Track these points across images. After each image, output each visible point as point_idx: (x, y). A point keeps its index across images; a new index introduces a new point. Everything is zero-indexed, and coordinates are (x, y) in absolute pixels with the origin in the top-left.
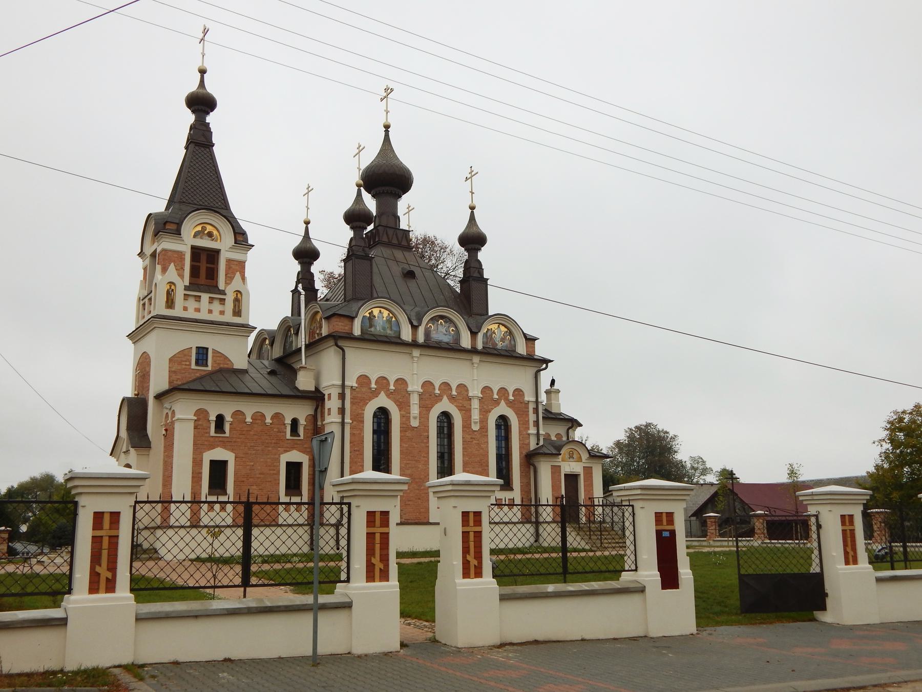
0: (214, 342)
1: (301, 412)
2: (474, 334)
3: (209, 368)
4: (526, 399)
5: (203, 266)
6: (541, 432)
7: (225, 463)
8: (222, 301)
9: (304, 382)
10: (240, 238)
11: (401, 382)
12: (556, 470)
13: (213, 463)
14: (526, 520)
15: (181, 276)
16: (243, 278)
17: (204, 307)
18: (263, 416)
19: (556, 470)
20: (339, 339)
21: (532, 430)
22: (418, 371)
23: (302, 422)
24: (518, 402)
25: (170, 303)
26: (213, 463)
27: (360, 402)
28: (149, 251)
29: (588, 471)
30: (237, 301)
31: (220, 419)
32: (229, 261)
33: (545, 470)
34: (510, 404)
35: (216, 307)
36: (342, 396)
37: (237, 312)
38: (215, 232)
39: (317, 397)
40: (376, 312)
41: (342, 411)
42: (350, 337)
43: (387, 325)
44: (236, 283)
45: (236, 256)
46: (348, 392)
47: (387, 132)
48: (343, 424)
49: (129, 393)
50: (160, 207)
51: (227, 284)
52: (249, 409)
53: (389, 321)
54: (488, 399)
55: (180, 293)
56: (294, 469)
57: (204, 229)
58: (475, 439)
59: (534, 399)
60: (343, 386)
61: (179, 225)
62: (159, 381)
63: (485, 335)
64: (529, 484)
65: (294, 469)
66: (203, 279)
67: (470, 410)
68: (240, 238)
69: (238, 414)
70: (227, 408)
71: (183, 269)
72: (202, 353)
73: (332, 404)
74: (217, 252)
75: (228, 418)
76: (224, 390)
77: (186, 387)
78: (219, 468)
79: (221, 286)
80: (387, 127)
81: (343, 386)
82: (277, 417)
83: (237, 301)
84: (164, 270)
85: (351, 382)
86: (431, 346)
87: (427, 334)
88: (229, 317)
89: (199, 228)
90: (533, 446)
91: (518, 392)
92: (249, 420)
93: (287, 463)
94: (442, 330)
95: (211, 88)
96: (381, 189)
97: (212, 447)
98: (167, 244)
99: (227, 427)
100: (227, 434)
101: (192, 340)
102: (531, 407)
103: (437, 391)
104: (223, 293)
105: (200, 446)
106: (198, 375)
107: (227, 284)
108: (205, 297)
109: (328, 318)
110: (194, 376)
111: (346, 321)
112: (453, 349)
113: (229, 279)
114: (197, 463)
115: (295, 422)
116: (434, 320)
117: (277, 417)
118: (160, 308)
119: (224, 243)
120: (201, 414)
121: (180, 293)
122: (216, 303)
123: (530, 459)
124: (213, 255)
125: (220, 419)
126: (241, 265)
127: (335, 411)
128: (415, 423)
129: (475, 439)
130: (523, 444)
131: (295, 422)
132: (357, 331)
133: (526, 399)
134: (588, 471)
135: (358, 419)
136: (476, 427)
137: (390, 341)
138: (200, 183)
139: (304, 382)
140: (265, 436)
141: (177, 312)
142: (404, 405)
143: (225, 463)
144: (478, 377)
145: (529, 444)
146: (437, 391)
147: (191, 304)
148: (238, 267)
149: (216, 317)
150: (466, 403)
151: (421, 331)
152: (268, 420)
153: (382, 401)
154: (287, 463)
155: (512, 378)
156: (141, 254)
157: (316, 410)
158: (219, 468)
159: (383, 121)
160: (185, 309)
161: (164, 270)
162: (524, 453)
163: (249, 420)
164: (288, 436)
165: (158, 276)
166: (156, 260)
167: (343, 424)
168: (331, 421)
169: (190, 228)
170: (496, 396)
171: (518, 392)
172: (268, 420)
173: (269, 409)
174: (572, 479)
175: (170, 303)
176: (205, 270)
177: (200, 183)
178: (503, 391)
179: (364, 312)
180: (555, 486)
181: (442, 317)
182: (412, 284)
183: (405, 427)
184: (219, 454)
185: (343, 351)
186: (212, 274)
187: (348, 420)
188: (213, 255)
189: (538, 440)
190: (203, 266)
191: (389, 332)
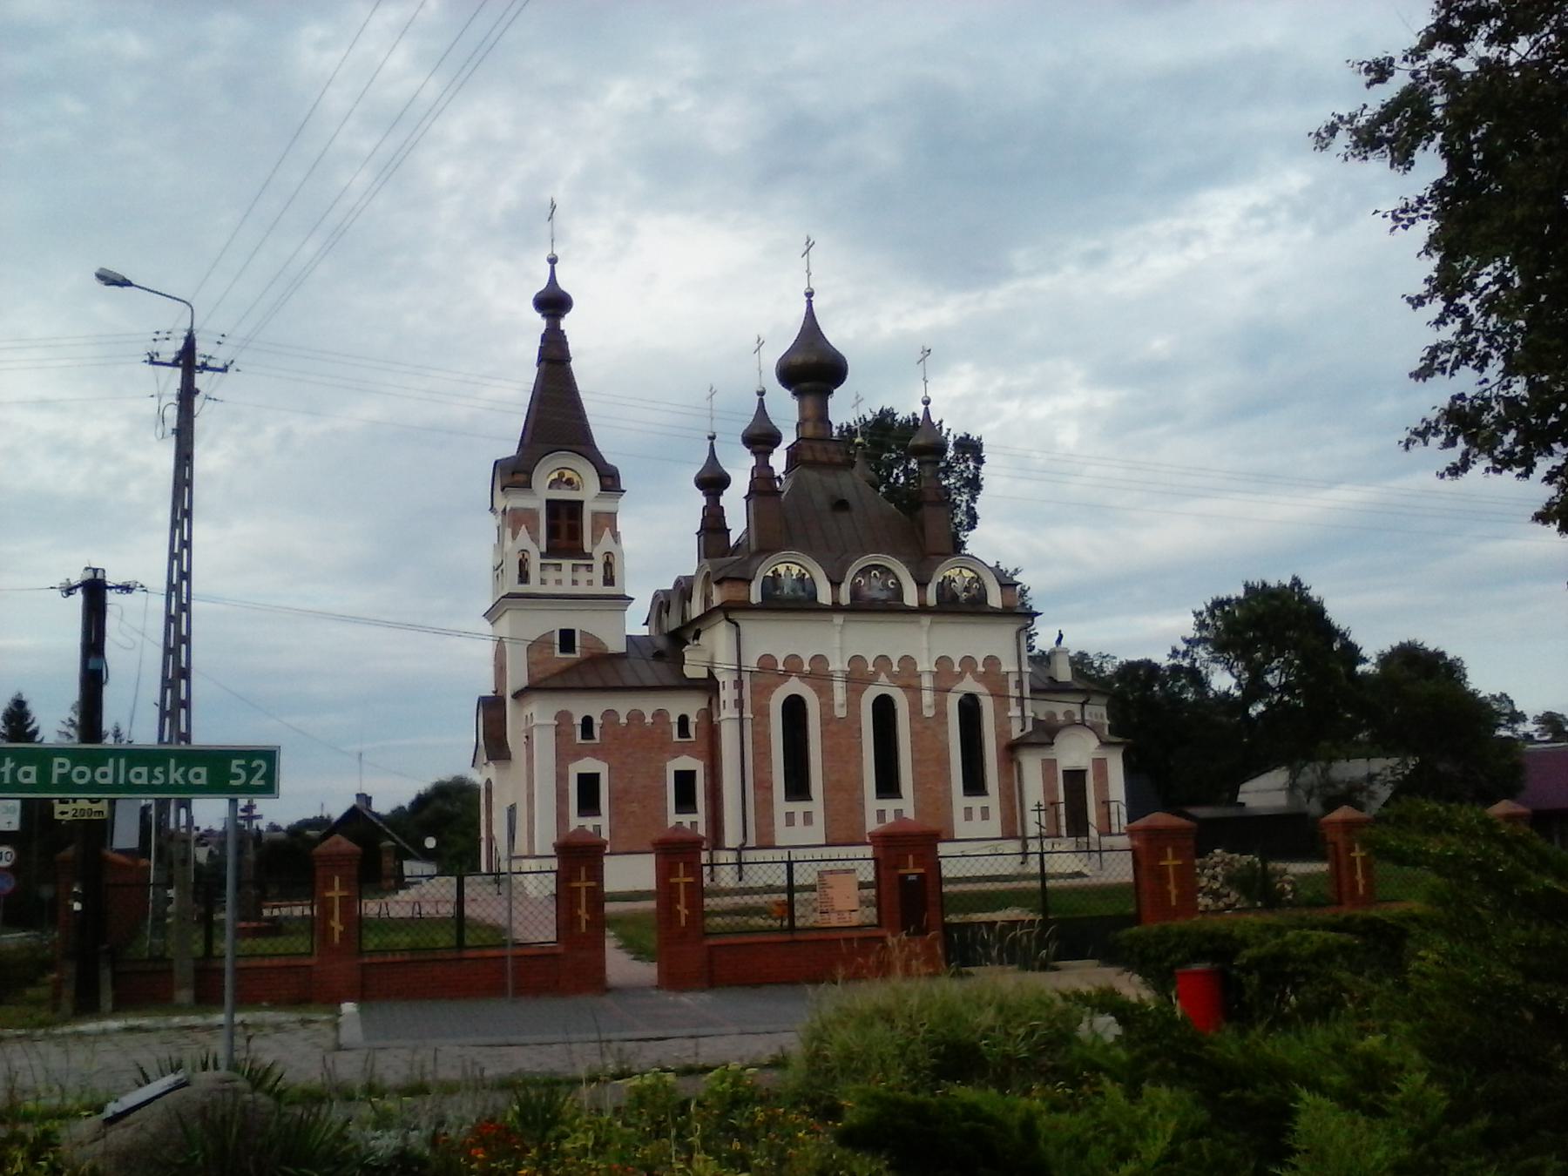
0: (582, 621)
1: (691, 706)
2: (922, 585)
3: (578, 655)
4: (1004, 669)
5: (564, 524)
6: (1029, 713)
7: (692, 774)
8: (589, 567)
9: (694, 669)
10: (610, 481)
11: (819, 659)
12: (1049, 766)
13: (581, 777)
14: (1009, 835)
15: (535, 540)
16: (616, 536)
17: (564, 577)
18: (641, 715)
19: (1049, 766)
20: (731, 610)
21: (1015, 712)
22: (839, 643)
23: (693, 719)
24: (992, 672)
25: (524, 577)
26: (581, 777)
27: (762, 693)
28: (499, 506)
29: (1100, 765)
30: (608, 565)
31: (587, 723)
32: (595, 515)
33: (1031, 765)
34: (980, 678)
35: (583, 575)
36: (739, 684)
37: (609, 580)
38: (576, 479)
39: (709, 686)
40: (782, 569)
41: (739, 703)
42: (746, 607)
43: (799, 586)
44: (606, 542)
45: (605, 506)
46: (746, 678)
47: (810, 303)
48: (741, 719)
49: (488, 691)
50: (510, 449)
51: (594, 543)
52: (623, 706)
53: (801, 578)
54: (945, 672)
55: (535, 562)
56: (685, 781)
57: (561, 475)
58: (927, 730)
59: (1016, 669)
60: (739, 670)
61: (529, 473)
62: (517, 677)
63: (941, 586)
64: (1011, 786)
65: (685, 781)
66: (563, 541)
67: (920, 689)
68: (609, 482)
69: (609, 714)
70: (593, 707)
71: (537, 529)
72: (567, 638)
73: (727, 694)
74: (581, 502)
75: (597, 721)
76: (611, 684)
77: (543, 685)
78: (588, 784)
79: (587, 548)
80: (810, 295)
81: (739, 670)
82: (660, 715)
83: (608, 565)
84: (514, 535)
85: (751, 662)
86: (861, 607)
87: (855, 592)
88: (599, 588)
89: (555, 476)
90: (1016, 733)
91: (992, 661)
92: (623, 720)
93: (677, 772)
94: (877, 584)
95: (564, 284)
96: (806, 385)
97: (578, 756)
98: (519, 501)
99: (597, 731)
100: (597, 741)
101: (552, 622)
102: (1012, 680)
103: (871, 668)
104: (590, 556)
105: (565, 754)
106: (564, 664)
107: (594, 543)
108: (567, 564)
109: (719, 583)
110: (555, 668)
111: (741, 586)
112: (892, 607)
113: (596, 538)
114: (561, 778)
115: (683, 721)
116: (865, 571)
117: (660, 715)
118: (512, 584)
119: (589, 490)
120: (563, 718)
121: (535, 562)
122: (582, 570)
123: (1011, 750)
124: (575, 508)
125: (587, 723)
126: (611, 518)
127: (730, 704)
128: (840, 712)
129: (927, 730)
130: (1002, 731)
131: (683, 721)
132: (755, 596)
133: (1004, 669)
134: (1100, 765)
135: (762, 713)
136: (929, 713)
137: (801, 604)
138: (557, 417)
139: (694, 669)
140: (637, 742)
141: (534, 586)
142: (824, 691)
143: (692, 774)
144: (926, 644)
145: (1010, 732)
146: (871, 668)
147: (551, 575)
148: (607, 521)
149: (582, 589)
150: (914, 682)
151: (845, 589)
152: (649, 720)
153: (794, 686)
154: (677, 772)
155: (988, 642)
156: (492, 509)
157: (710, 703)
158: (588, 784)
159: (804, 288)
160: (543, 582)
161: (514, 535)
162: (1004, 743)
163: (623, 720)
164: (676, 738)
165: (509, 543)
166: (515, 520)
167: (741, 719)
168: (727, 715)
169: (543, 476)
170: (957, 669)
171: (992, 661)
172: (649, 720)
173: (648, 706)
174: (1075, 778)
175: (524, 577)
176: (565, 530)
177: (557, 417)
178: (968, 661)
179: (764, 570)
180: (1049, 788)
181: (875, 567)
182: (843, 516)
183: (827, 719)
184: (589, 765)
185: (737, 625)
186: (575, 533)
187: (748, 714)
188: (575, 508)
189: (1024, 724)
190: (564, 524)
191: (801, 594)
